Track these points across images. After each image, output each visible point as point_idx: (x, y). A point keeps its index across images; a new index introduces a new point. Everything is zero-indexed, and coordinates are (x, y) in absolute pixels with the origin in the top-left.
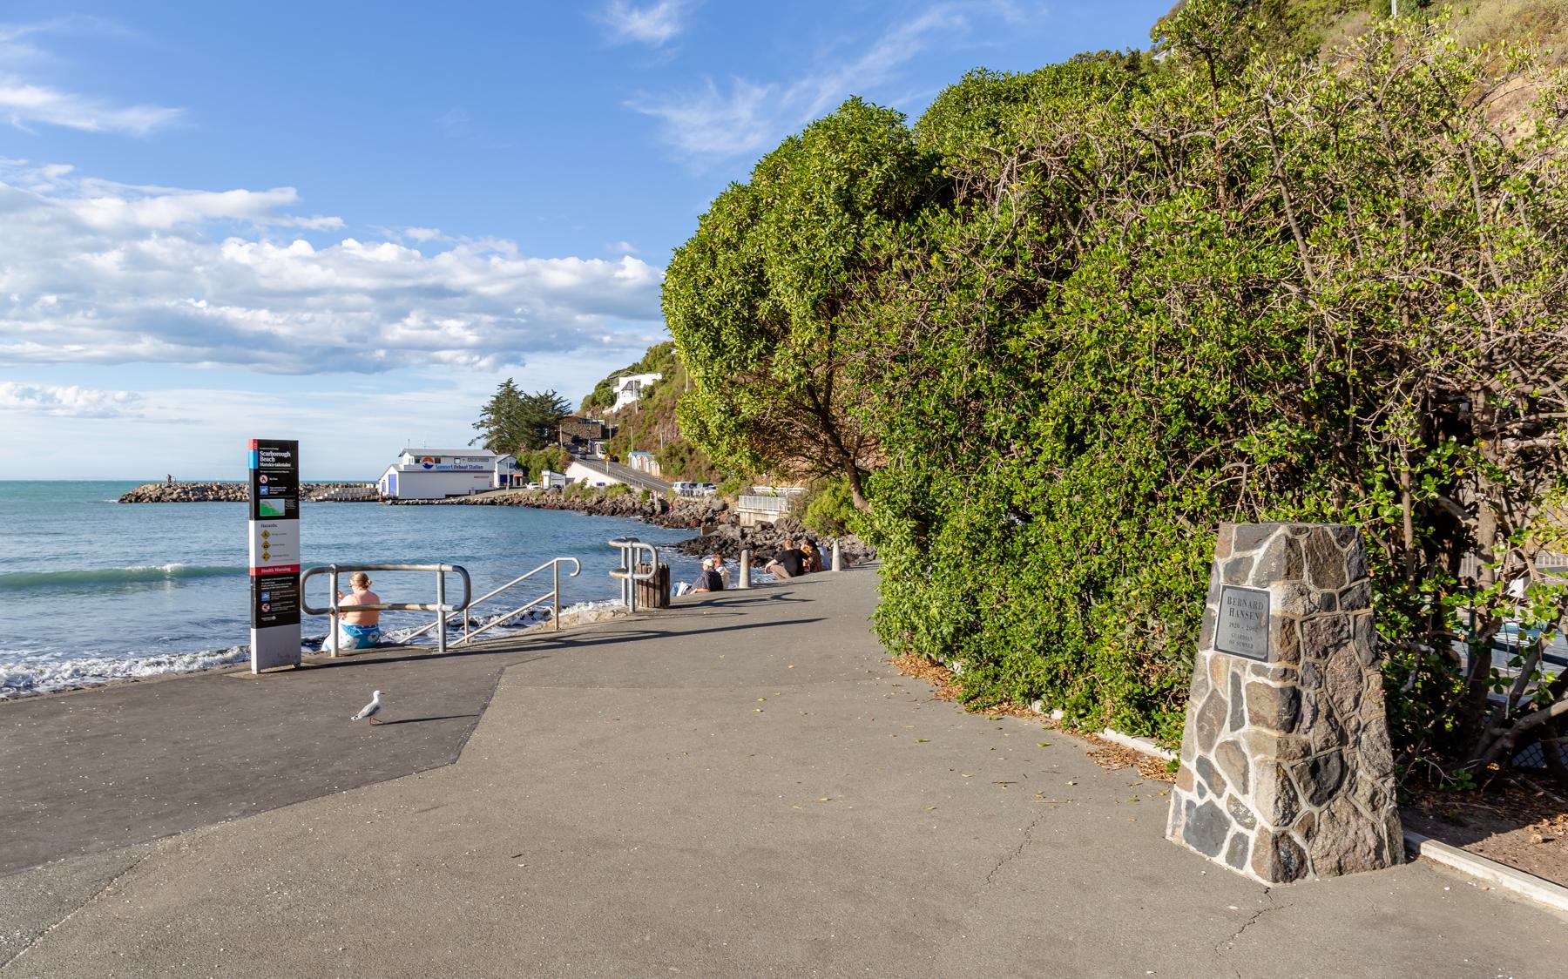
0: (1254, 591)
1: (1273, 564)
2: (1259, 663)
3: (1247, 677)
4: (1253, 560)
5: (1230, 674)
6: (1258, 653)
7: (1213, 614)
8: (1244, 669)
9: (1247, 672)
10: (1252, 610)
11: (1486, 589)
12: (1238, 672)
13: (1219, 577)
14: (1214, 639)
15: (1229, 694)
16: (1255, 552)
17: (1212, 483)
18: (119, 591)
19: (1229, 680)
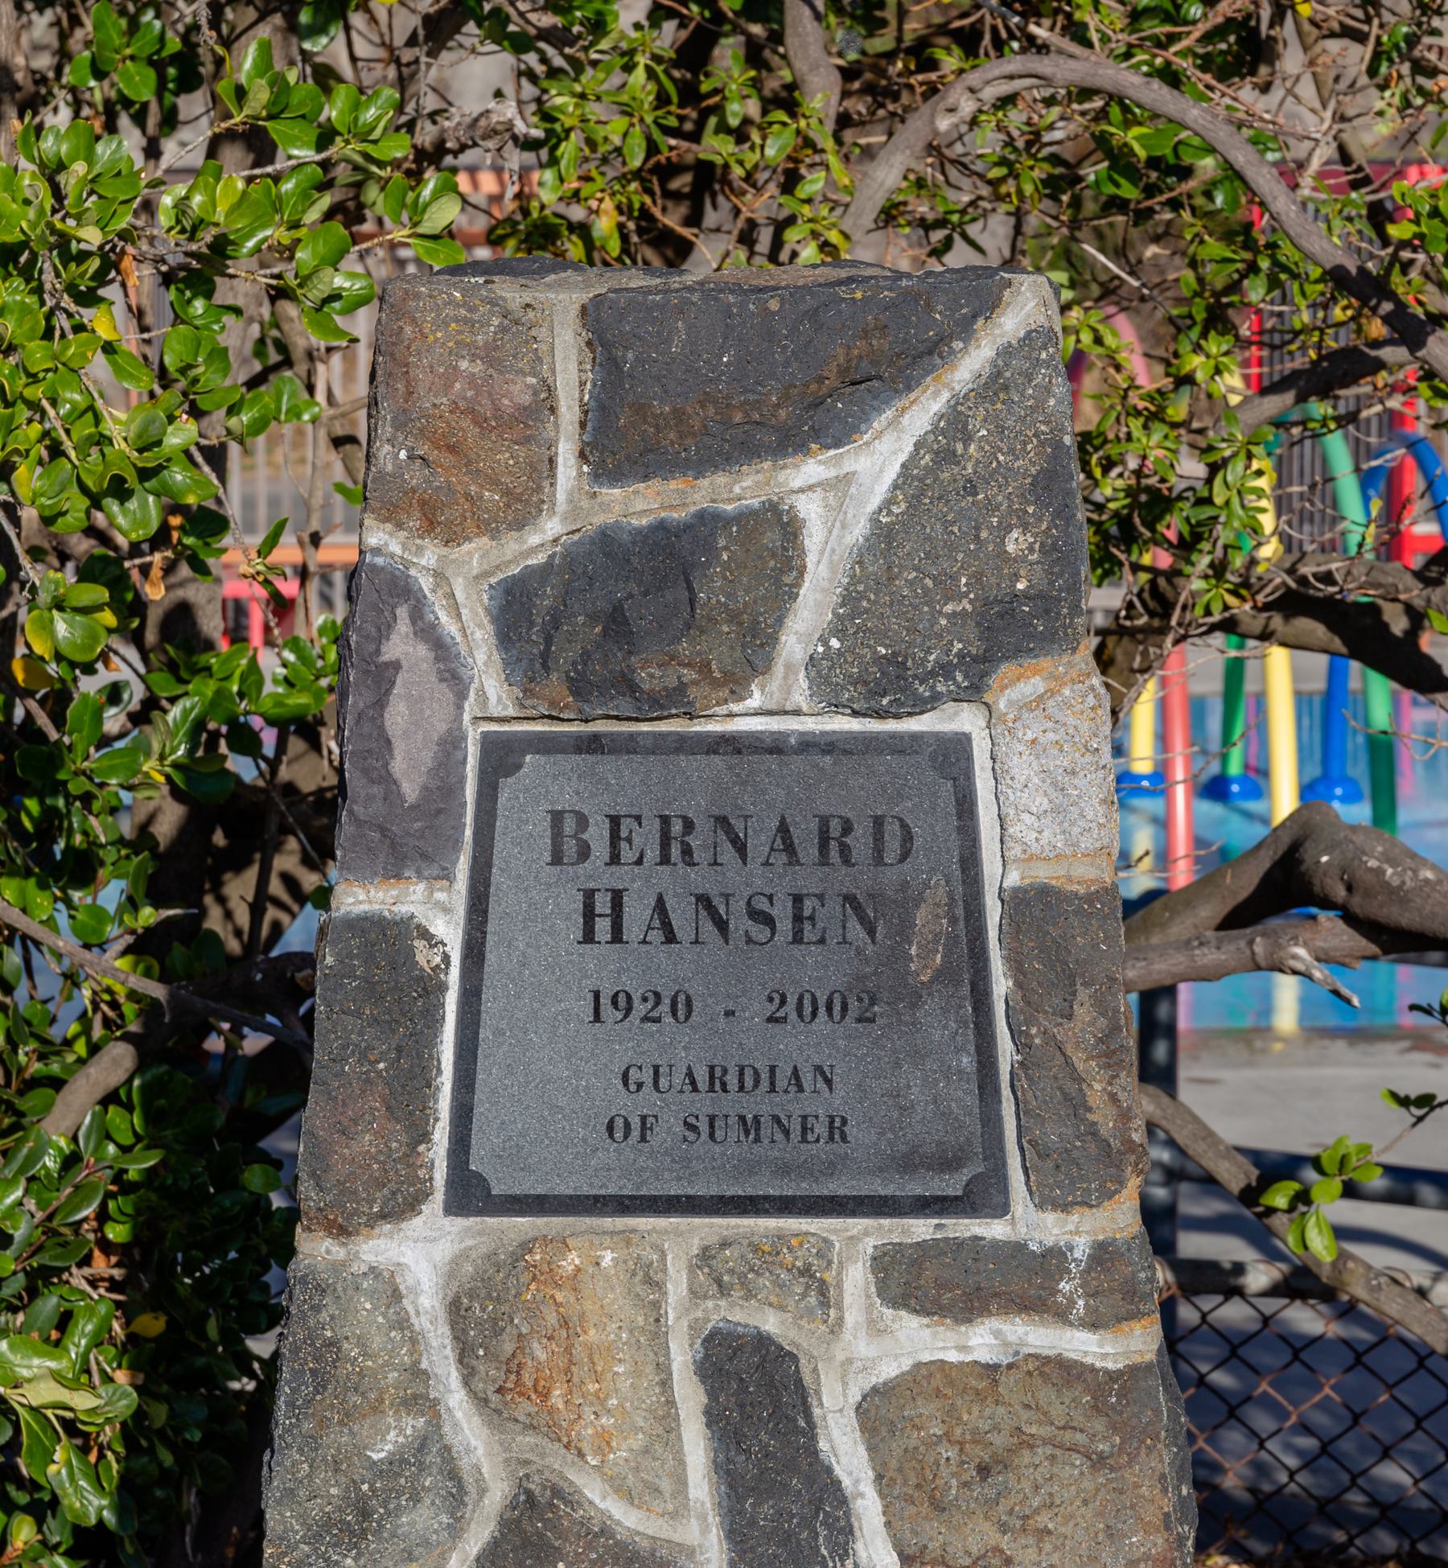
0: (829, 745)
1: (1017, 540)
2: (921, 1229)
3: (856, 1342)
4: (791, 529)
5: (681, 1357)
6: (909, 1163)
7: (425, 957)
8: (825, 1295)
9: (853, 1316)
10: (808, 879)
11: (1264, 98)
12: (771, 1323)
13: (454, 678)
14: (441, 1135)
15: (701, 1486)
16: (812, 469)
17: (1032, 168)
18: (1363, 1047)
19: (690, 1397)
